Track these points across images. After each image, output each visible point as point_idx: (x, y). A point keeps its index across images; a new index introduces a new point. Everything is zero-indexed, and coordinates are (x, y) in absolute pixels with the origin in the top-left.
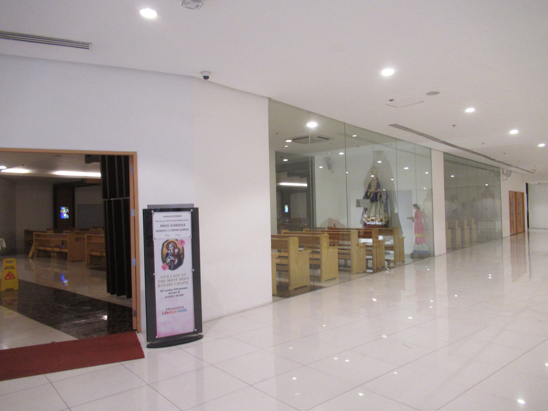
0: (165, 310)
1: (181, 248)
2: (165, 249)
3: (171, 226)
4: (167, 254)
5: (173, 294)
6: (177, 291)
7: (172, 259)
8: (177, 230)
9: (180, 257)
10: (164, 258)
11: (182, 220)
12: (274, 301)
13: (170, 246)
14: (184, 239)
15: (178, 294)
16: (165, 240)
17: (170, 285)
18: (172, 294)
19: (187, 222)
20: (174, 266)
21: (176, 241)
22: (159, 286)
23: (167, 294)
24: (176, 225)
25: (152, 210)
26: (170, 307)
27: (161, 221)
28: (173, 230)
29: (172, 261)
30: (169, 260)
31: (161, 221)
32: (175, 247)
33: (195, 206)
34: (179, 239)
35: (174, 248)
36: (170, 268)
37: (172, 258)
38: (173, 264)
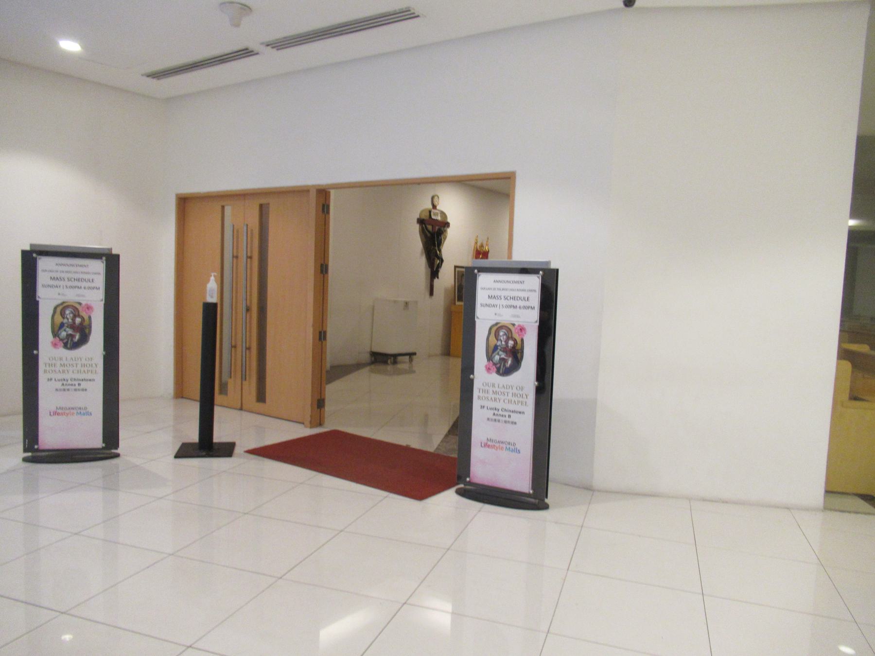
0: (53, 409)
1: (86, 318)
2: (492, 338)
3: (506, 298)
4: (62, 325)
5: (501, 418)
6: (507, 414)
7: (503, 356)
8: (515, 307)
9: (516, 354)
10: (490, 353)
11: (88, 273)
12: (827, 508)
13: (501, 334)
14: (93, 304)
15: (507, 419)
16: (494, 322)
17: (64, 372)
18: (66, 386)
19: (533, 293)
20: (72, 344)
21: (511, 327)
22: (45, 371)
23: (59, 385)
24: (514, 298)
25: (475, 268)
26: (494, 438)
27: (489, 289)
28: (507, 306)
29: (502, 359)
30: (497, 358)
31: (489, 289)
32: (76, 313)
33: (114, 252)
34: (517, 324)
35: (75, 316)
36: (66, 346)
37: (70, 332)
38: (72, 340)
